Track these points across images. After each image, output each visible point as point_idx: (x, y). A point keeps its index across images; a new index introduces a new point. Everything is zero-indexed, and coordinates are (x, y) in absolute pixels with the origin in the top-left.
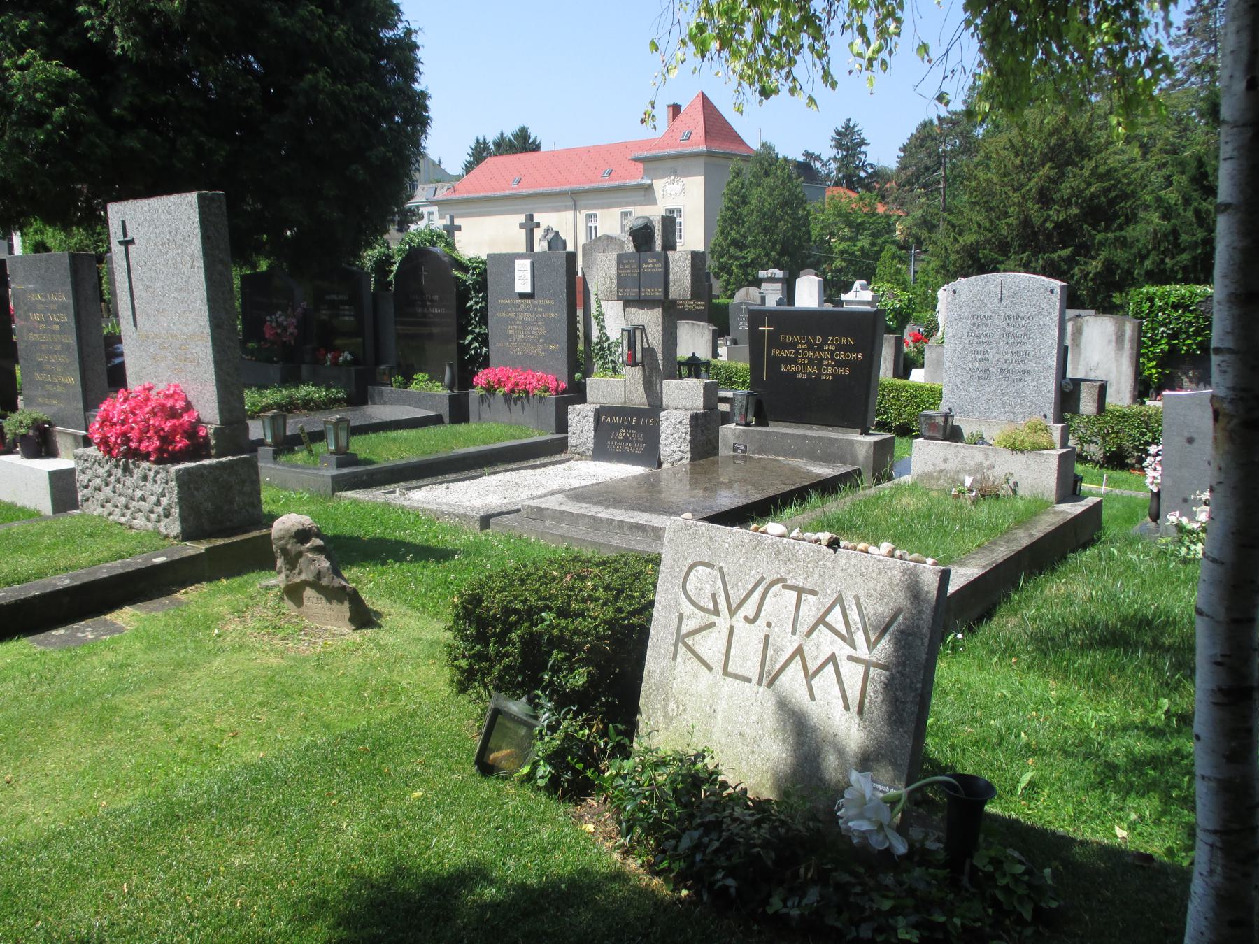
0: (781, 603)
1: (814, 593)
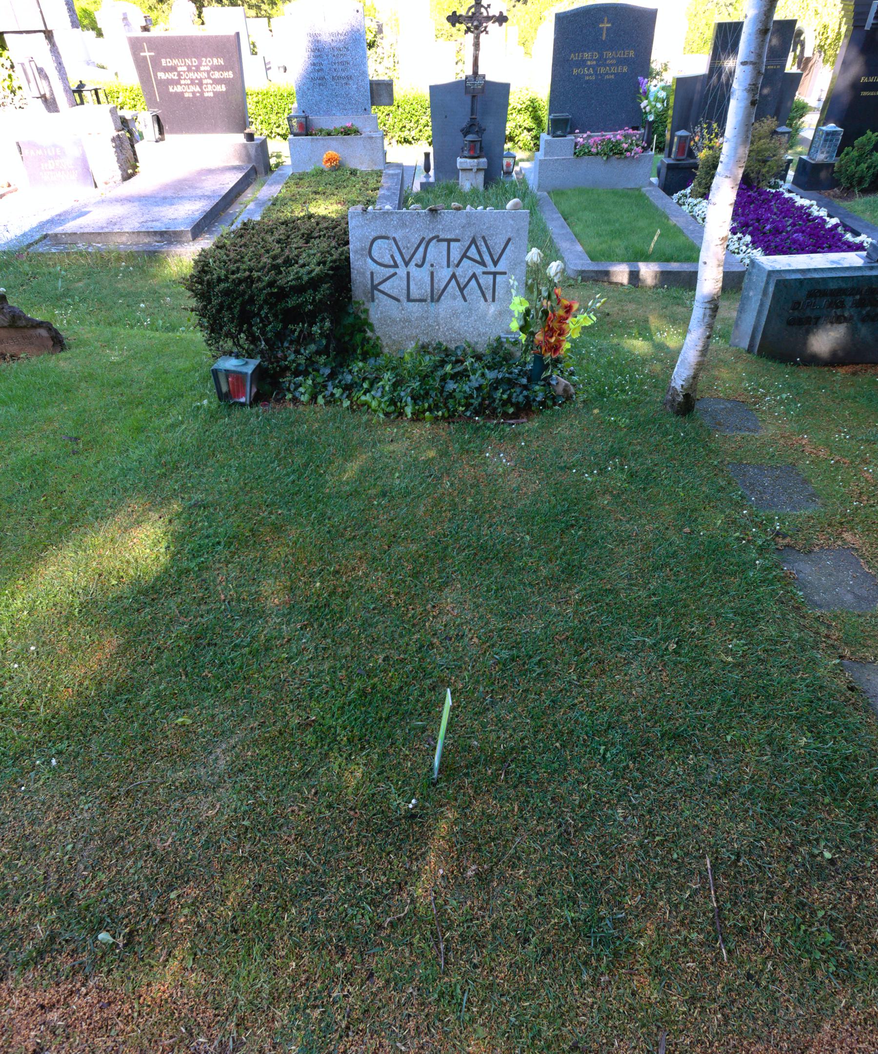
0: (437, 252)
1: (457, 240)
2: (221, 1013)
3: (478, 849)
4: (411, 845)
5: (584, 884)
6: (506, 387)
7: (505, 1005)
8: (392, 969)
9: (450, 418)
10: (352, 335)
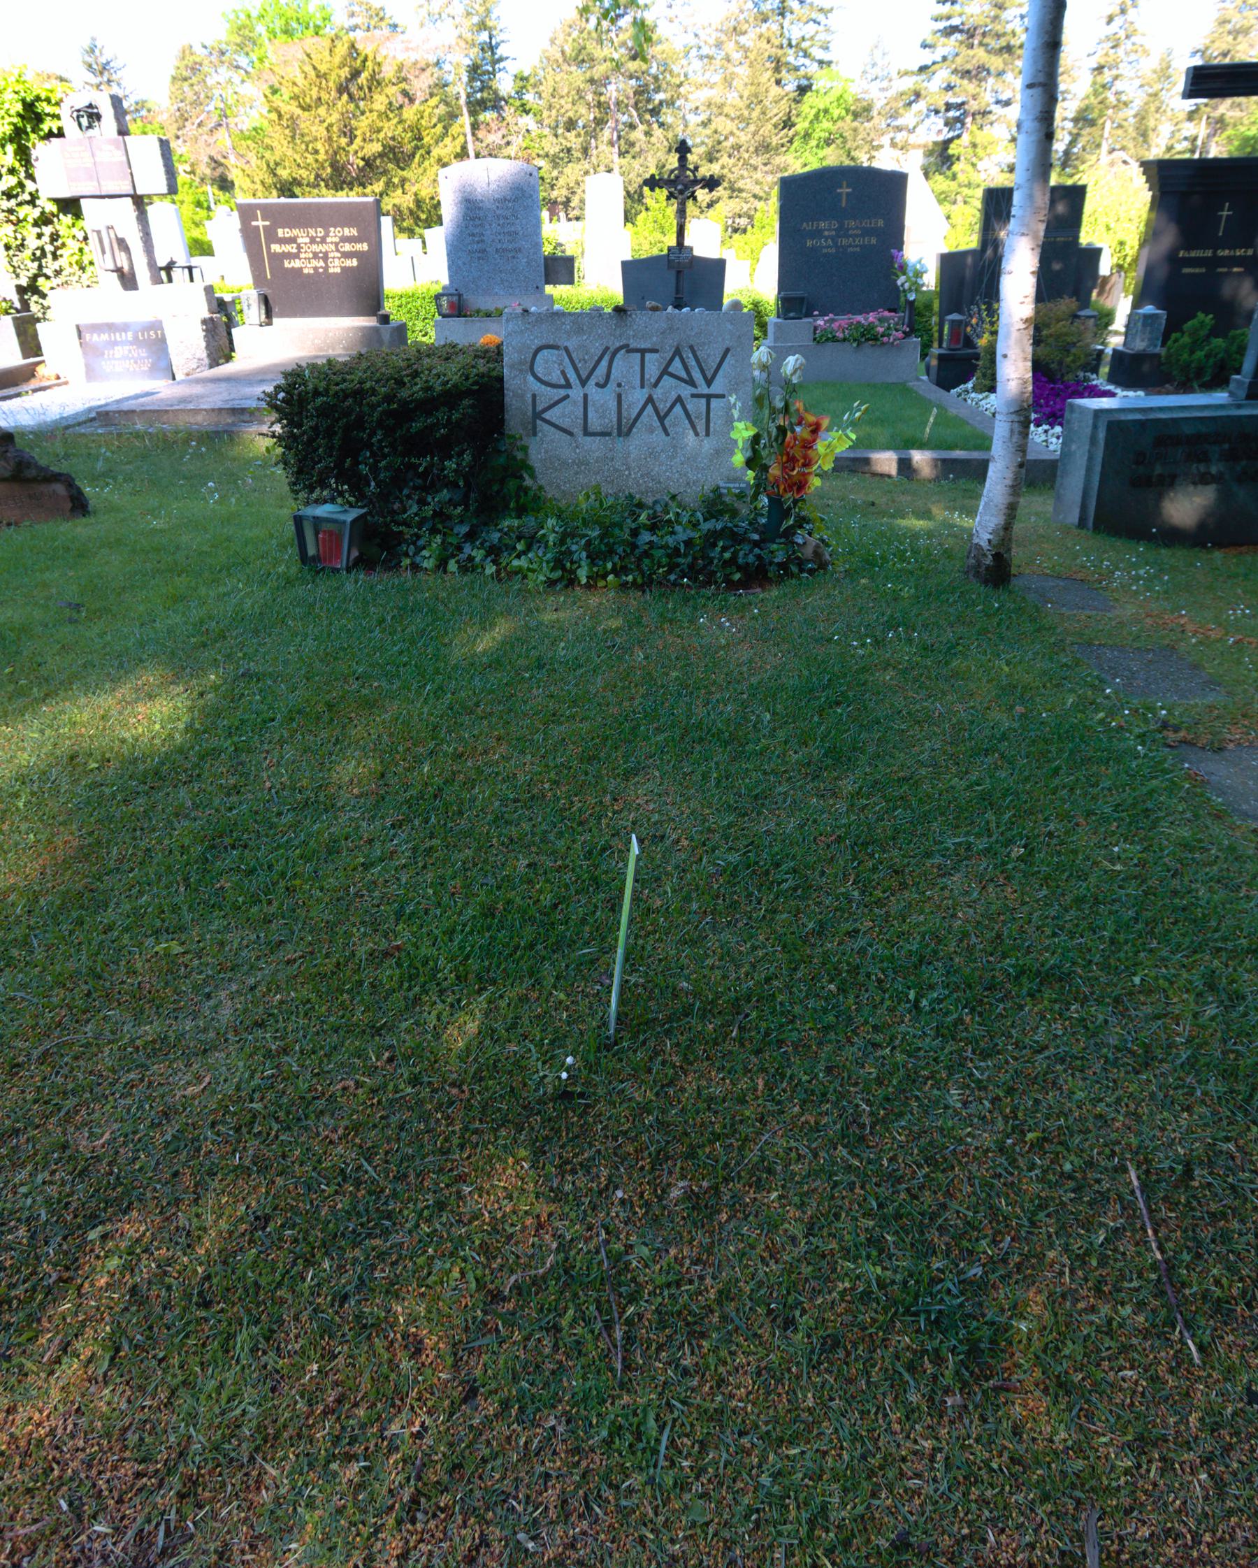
0: (625, 367)
2: (151, 1469)
3: (691, 1154)
4: (562, 1147)
5: (898, 1216)
6: (729, 543)
7: (749, 1455)
8: (516, 1379)
9: (644, 585)
10: (502, 481)
